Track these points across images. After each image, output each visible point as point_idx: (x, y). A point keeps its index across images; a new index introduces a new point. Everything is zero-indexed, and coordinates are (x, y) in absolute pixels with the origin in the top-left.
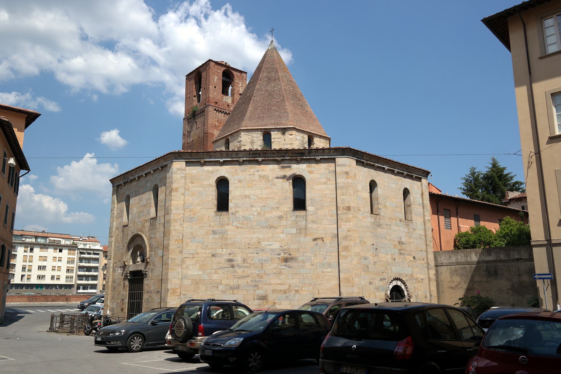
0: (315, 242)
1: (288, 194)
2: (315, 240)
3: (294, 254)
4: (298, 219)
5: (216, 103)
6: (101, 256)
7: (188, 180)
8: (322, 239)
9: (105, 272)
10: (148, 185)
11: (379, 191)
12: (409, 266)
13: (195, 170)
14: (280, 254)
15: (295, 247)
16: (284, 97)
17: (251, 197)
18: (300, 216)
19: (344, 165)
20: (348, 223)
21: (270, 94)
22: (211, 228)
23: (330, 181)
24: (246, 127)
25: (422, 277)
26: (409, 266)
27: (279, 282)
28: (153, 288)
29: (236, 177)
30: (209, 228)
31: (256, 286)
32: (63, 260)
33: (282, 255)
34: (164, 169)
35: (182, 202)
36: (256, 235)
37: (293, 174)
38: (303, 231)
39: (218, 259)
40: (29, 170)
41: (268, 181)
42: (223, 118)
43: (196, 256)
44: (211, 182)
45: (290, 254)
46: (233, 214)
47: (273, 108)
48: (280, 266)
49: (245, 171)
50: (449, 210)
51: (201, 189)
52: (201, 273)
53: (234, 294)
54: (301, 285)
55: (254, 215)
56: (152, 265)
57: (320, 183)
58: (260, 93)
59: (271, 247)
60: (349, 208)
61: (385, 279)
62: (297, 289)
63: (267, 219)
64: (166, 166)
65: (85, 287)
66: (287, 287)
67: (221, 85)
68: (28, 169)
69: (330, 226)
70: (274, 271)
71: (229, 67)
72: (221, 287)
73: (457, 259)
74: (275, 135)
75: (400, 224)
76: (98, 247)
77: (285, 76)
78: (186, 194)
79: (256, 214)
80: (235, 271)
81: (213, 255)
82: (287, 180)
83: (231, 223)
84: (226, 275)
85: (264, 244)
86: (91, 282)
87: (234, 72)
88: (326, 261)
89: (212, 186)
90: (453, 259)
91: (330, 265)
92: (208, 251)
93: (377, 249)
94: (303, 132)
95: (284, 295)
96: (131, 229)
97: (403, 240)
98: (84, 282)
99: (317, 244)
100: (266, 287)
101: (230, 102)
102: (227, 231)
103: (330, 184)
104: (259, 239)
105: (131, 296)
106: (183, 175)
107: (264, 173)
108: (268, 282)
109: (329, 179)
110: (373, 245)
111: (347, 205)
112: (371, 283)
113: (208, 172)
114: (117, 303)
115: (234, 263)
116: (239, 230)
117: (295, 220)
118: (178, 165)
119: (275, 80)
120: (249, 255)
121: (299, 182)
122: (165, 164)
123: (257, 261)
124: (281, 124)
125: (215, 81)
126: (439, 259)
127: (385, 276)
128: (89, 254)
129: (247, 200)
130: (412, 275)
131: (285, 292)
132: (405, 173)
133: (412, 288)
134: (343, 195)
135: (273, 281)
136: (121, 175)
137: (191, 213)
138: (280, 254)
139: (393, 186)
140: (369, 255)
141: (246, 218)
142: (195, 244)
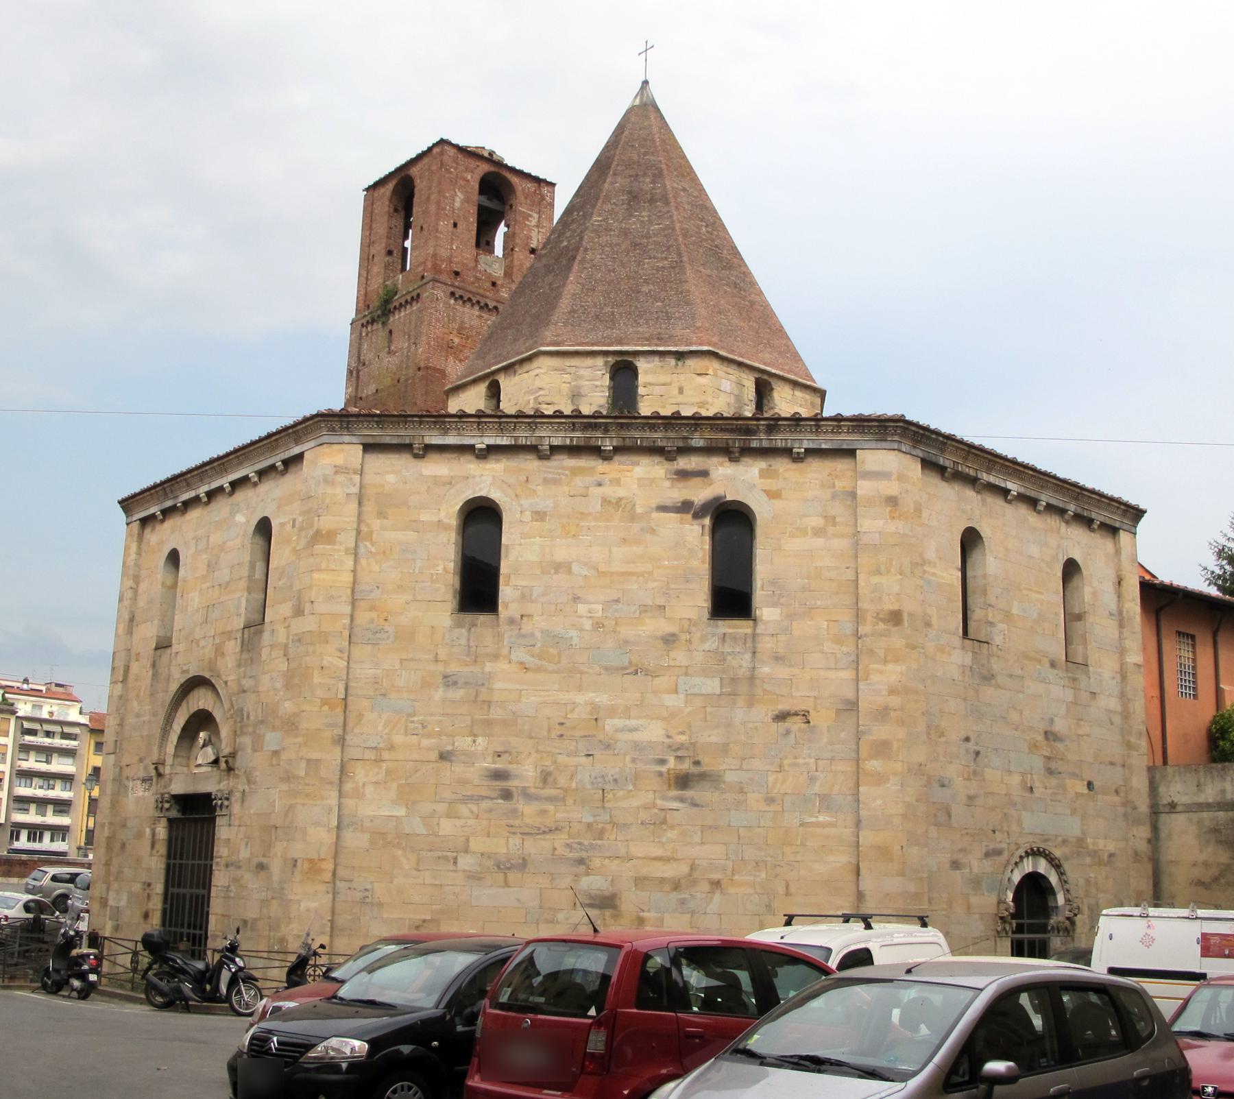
0: (782, 726)
1: (695, 563)
2: (782, 717)
3: (708, 764)
4: (727, 649)
5: (457, 273)
6: (84, 744)
8: (805, 715)
9: (96, 793)
10: (240, 518)
11: (989, 563)
12: (1074, 812)
13: (392, 472)
14: (662, 762)
15: (714, 739)
16: (680, 255)
18: (734, 638)
19: (884, 475)
20: (890, 666)
21: (635, 245)
22: (440, 668)
23: (835, 524)
24: (557, 344)
25: (1111, 847)
26: (1074, 812)
27: (659, 852)
28: (244, 854)
29: (526, 503)
30: (432, 667)
31: (581, 861)
33: (672, 763)
34: (292, 469)
35: (347, 578)
36: (589, 696)
37: (717, 499)
38: (741, 687)
39: (458, 768)
41: (633, 517)
42: (476, 322)
43: (386, 755)
44: (443, 514)
45: (697, 763)
46: (511, 621)
47: (645, 289)
48: (664, 798)
49: (556, 482)
50: (1193, 637)
51: (411, 536)
52: (401, 812)
53: (507, 885)
54: (730, 863)
55: (581, 630)
56: (243, 779)
57: (803, 532)
58: (603, 239)
59: (636, 736)
60: (895, 617)
61: (998, 853)
63: (626, 642)
64: (299, 457)
65: (35, 832)
66: (684, 869)
67: (473, 219)
69: (832, 674)
70: (644, 816)
71: (500, 164)
72: (465, 862)
73: (1223, 791)
74: (648, 373)
75: (1051, 674)
76: (73, 715)
77: (684, 190)
78: (362, 551)
79: (588, 625)
80: (514, 811)
81: (444, 756)
82: (697, 516)
83: (505, 651)
84: (484, 823)
85: (611, 724)
86: (51, 819)
87: (515, 180)
88: (817, 788)
90: (1210, 794)
91: (826, 802)
92: (426, 742)
93: (977, 753)
95: (674, 895)
96: (180, 660)
97: (1060, 726)
98: (32, 817)
99: (788, 732)
100: (614, 866)
102: (490, 676)
103: (836, 536)
104: (595, 708)
105: (173, 875)
107: (621, 492)
108: (623, 852)
109: (832, 520)
110: (967, 739)
111: (890, 605)
112: (955, 865)
113: (436, 481)
114: (131, 895)
115: (512, 784)
116: (530, 675)
117: (716, 651)
118: (331, 458)
119: (652, 201)
120: (562, 759)
121: (731, 523)
122: (296, 450)
123: (587, 780)
124: (670, 339)
125: (457, 205)
126: (1162, 790)
127: (1000, 842)
128: (48, 734)
129: (561, 579)
130: (1081, 841)
131: (676, 886)
132: (1072, 508)
133: (1081, 882)
134: (878, 572)
135: (638, 850)
137: (374, 614)
139: (1034, 550)
140: (952, 771)
141: (557, 640)
142: (385, 716)
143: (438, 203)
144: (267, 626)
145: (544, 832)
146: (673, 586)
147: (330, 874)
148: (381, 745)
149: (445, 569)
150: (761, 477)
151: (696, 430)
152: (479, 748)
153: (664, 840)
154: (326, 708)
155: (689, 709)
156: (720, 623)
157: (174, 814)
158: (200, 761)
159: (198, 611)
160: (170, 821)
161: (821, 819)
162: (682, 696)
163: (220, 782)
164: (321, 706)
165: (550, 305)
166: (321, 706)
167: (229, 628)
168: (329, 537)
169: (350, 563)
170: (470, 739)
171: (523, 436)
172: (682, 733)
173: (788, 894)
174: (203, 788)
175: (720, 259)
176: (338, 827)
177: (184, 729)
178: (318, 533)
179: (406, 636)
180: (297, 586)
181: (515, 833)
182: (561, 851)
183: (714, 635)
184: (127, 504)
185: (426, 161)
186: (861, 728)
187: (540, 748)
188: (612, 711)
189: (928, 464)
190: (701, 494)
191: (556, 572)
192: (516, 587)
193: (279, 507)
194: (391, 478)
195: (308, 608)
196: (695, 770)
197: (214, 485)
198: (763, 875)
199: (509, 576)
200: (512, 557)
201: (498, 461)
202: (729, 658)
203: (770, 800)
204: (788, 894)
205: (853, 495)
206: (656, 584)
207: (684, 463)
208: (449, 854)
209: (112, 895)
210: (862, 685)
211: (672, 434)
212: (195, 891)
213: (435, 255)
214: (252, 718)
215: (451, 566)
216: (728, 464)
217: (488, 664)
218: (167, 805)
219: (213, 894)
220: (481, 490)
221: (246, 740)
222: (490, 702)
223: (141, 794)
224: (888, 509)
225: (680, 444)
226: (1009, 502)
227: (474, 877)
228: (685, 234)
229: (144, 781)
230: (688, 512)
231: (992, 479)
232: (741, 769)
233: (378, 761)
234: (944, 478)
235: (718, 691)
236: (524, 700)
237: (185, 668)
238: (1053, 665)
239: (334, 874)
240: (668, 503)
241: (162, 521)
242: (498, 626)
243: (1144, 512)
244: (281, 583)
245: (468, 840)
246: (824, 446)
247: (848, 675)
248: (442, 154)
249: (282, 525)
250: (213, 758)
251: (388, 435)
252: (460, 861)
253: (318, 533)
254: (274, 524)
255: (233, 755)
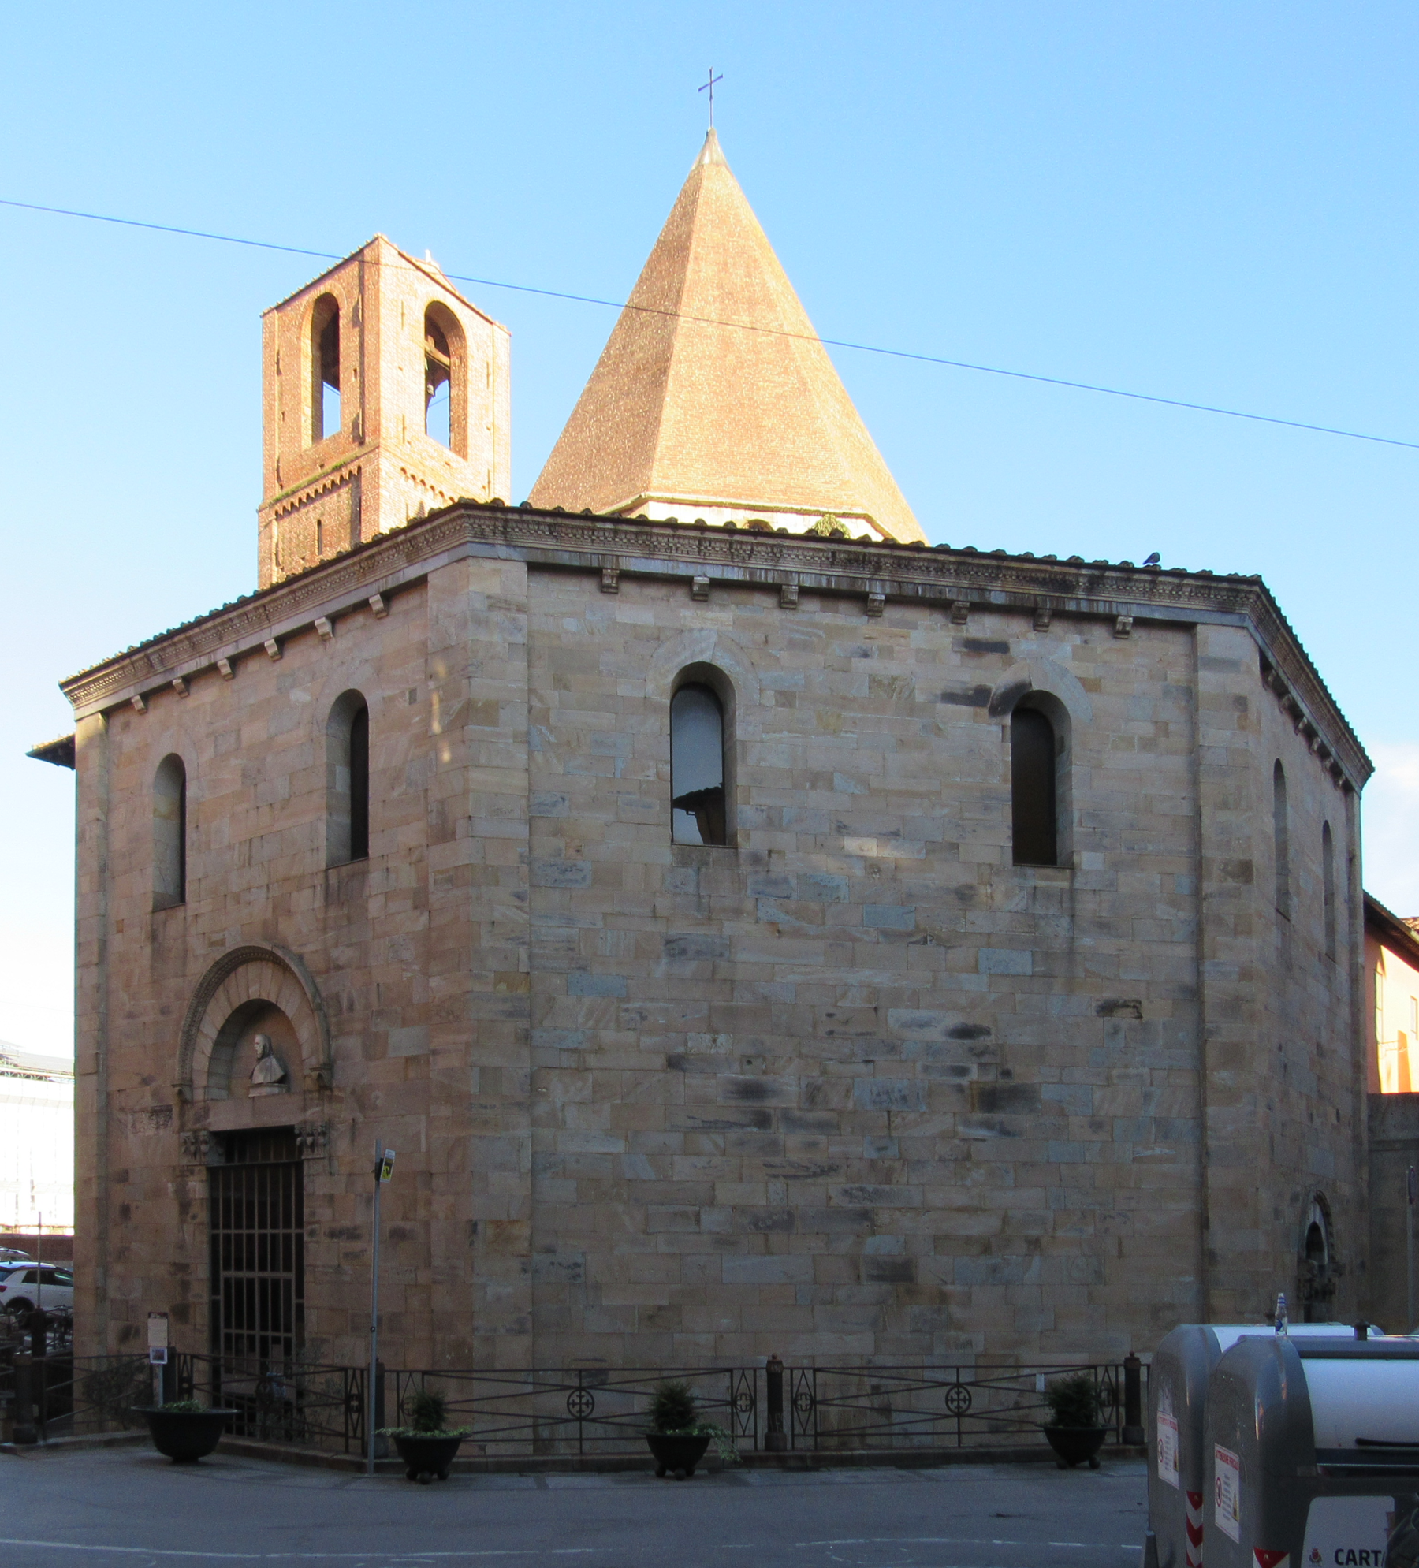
0: (1107, 1023)
2: (1108, 1008)
8: (1136, 1007)
10: (299, 695)
14: (962, 1071)
15: (1026, 1039)
17: (838, 780)
23: (1167, 734)
27: (960, 1200)
31: (865, 1215)
33: (974, 1074)
34: (399, 606)
36: (864, 975)
45: (1007, 1073)
46: (756, 859)
48: (967, 1123)
52: (619, 1147)
53: (769, 1252)
64: (421, 582)
72: (712, 1220)
80: (774, 1144)
81: (675, 1063)
82: (994, 712)
83: (749, 905)
85: (895, 1016)
88: (1152, 1110)
92: (647, 1041)
99: (1116, 1031)
107: (892, 668)
109: (1163, 728)
113: (637, 633)
115: (771, 1104)
122: (412, 573)
136: (133, 652)
137: (560, 843)
145: (815, 1175)
146: (967, 815)
147: (526, 1244)
148: (583, 1047)
149: (658, 774)
150: (1074, 659)
151: (997, 578)
152: (722, 1051)
153: (968, 1182)
154: (503, 987)
155: (993, 996)
156: (1029, 871)
157: (216, 1160)
159: (230, 847)
160: (212, 1172)
161: (1158, 1151)
162: (985, 978)
163: (304, 1109)
164: (496, 985)
166: (496, 985)
168: (488, 712)
169: (522, 756)
170: (708, 1037)
173: (1120, 1255)
176: (533, 1172)
177: (222, 1032)
178: (469, 706)
181: (776, 1176)
182: (838, 1200)
183: (1022, 888)
184: (63, 686)
186: (1208, 1026)
187: (804, 1051)
190: (999, 678)
191: (813, 786)
192: (759, 809)
193: (378, 671)
194: (570, 624)
195: (461, 827)
196: (1002, 1082)
197: (245, 645)
198: (1091, 1230)
201: (723, 607)
202: (1043, 923)
203: (1097, 1125)
206: (946, 811)
207: (984, 627)
208: (690, 1209)
209: (113, 1284)
210: (1207, 966)
212: (268, 1274)
214: (358, 1007)
216: (1032, 635)
217: (726, 923)
218: (204, 1148)
220: (702, 652)
222: (732, 981)
223: (151, 1132)
224: (1237, 714)
225: (975, 597)
227: (725, 1242)
229: (154, 1112)
230: (983, 705)
232: (1060, 1082)
233: (582, 1070)
235: (1029, 972)
236: (778, 979)
237: (216, 937)
240: (957, 689)
241: (142, 712)
242: (738, 866)
244: (395, 794)
245: (713, 1188)
246: (1157, 616)
247: (1185, 951)
249: (389, 701)
250: (279, 1073)
253: (469, 706)
254: (373, 700)
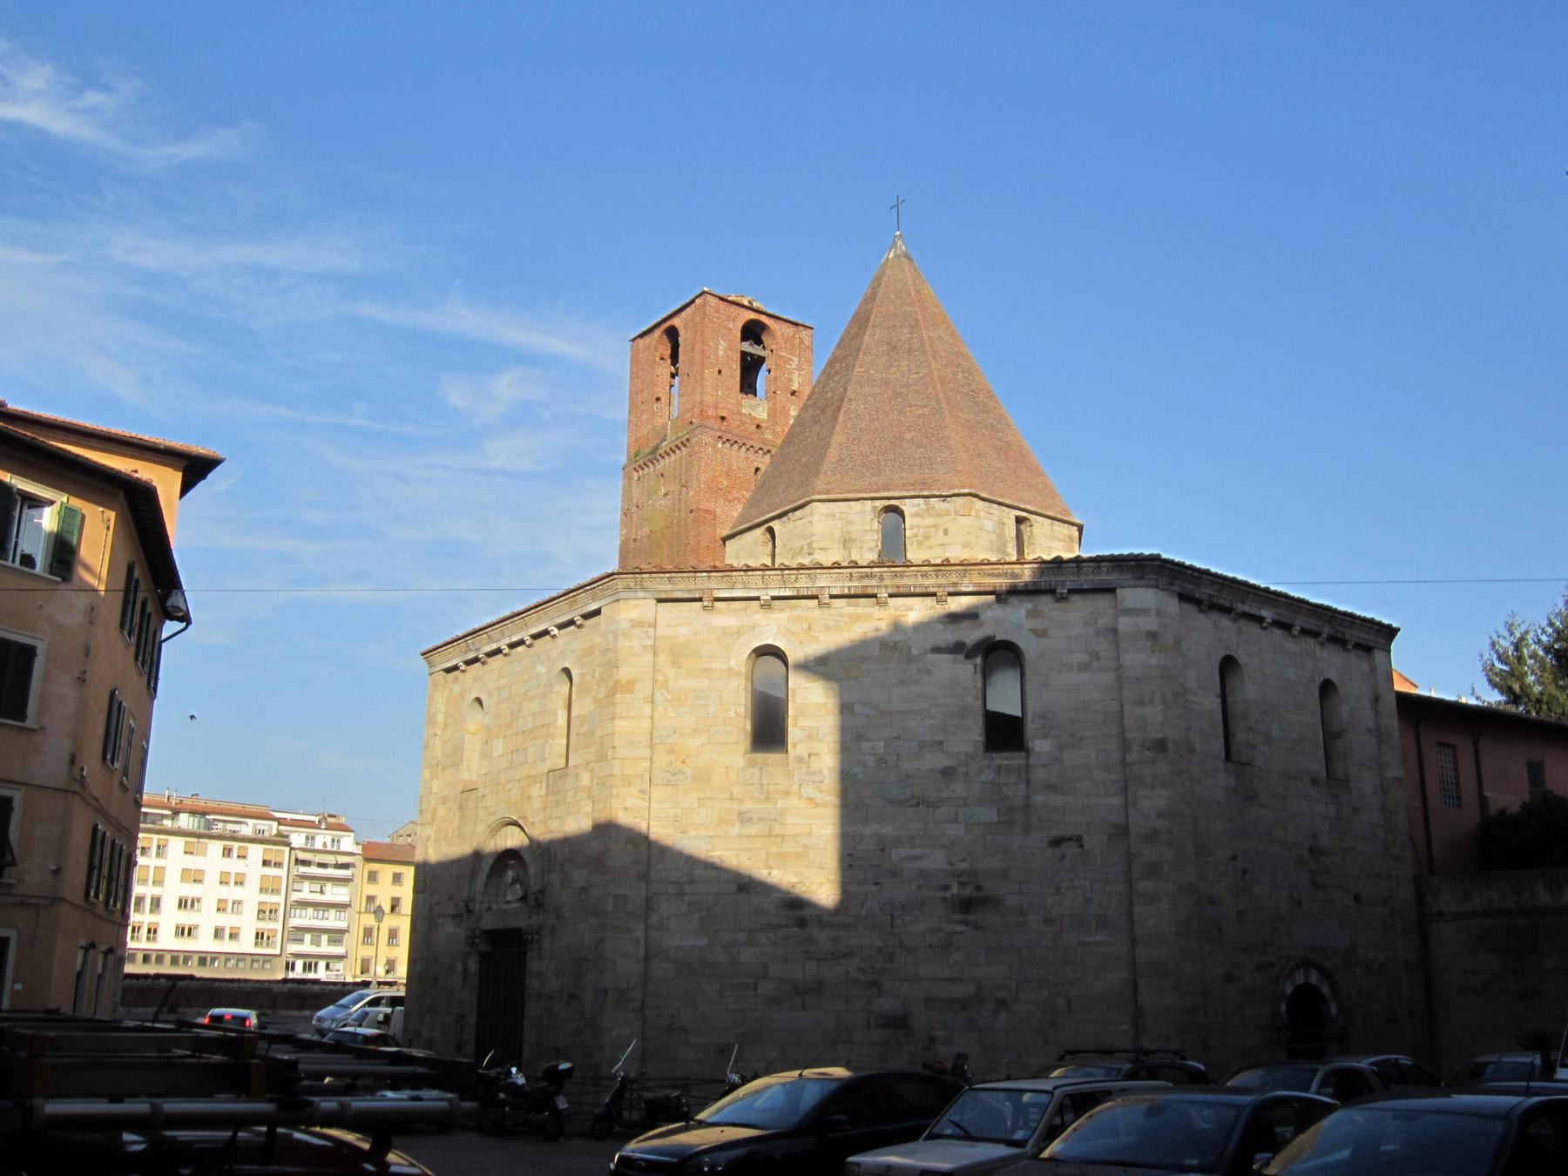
0: (1058, 851)
2: (1057, 842)
5: (723, 418)
7: (663, 659)
8: (1079, 840)
13: (681, 622)
16: (939, 401)
17: (857, 708)
18: (1009, 770)
21: (896, 395)
22: (735, 806)
24: (828, 492)
31: (874, 984)
32: (247, 881)
33: (955, 889)
35: (646, 724)
40: (189, 622)
41: (910, 659)
45: (979, 888)
46: (800, 760)
50: (1453, 747)
51: (703, 683)
52: (703, 942)
53: (804, 1007)
57: (1070, 667)
58: (866, 390)
60: (1160, 745)
62: (1001, 994)
63: (908, 776)
66: (972, 989)
68: (186, 619)
72: (765, 987)
77: (940, 338)
78: (658, 696)
79: (871, 761)
82: (970, 655)
83: (796, 787)
85: (896, 854)
86: (325, 948)
89: (737, 674)
94: (1073, 524)
98: (307, 947)
99: (1063, 856)
101: (764, 416)
106: (650, 642)
109: (1096, 655)
110: (1234, 858)
111: (1154, 734)
113: (725, 631)
118: (632, 611)
119: (910, 351)
124: (1048, 508)
125: (721, 353)
131: (964, 1004)
132: (1326, 630)
134: (1141, 703)
137: (672, 757)
138: (946, 888)
139: (1291, 673)
143: (703, 352)
144: (571, 770)
157: (484, 948)
158: (509, 898)
165: (819, 452)
167: (533, 772)
171: (804, 583)
172: (963, 860)
173: (1070, 1010)
174: (513, 923)
175: (977, 404)
179: (703, 777)
180: (599, 733)
185: (689, 310)
188: (898, 842)
189: (1184, 598)
196: (976, 895)
199: (796, 718)
200: (799, 700)
203: (1049, 921)
204: (1070, 1010)
205: (1115, 631)
210: (1131, 810)
211: (942, 581)
213: (701, 402)
215: (742, 710)
219: (526, 1024)
221: (555, 878)
223: (451, 930)
225: (951, 590)
226: (1265, 629)
228: (943, 382)
231: (1246, 608)
234: (1202, 611)
235: (995, 819)
238: (1314, 782)
239: (643, 1003)
240: (942, 644)
243: (1396, 630)
248: (704, 304)
250: (521, 894)
251: (682, 587)
252: (760, 988)
255: (542, 891)
